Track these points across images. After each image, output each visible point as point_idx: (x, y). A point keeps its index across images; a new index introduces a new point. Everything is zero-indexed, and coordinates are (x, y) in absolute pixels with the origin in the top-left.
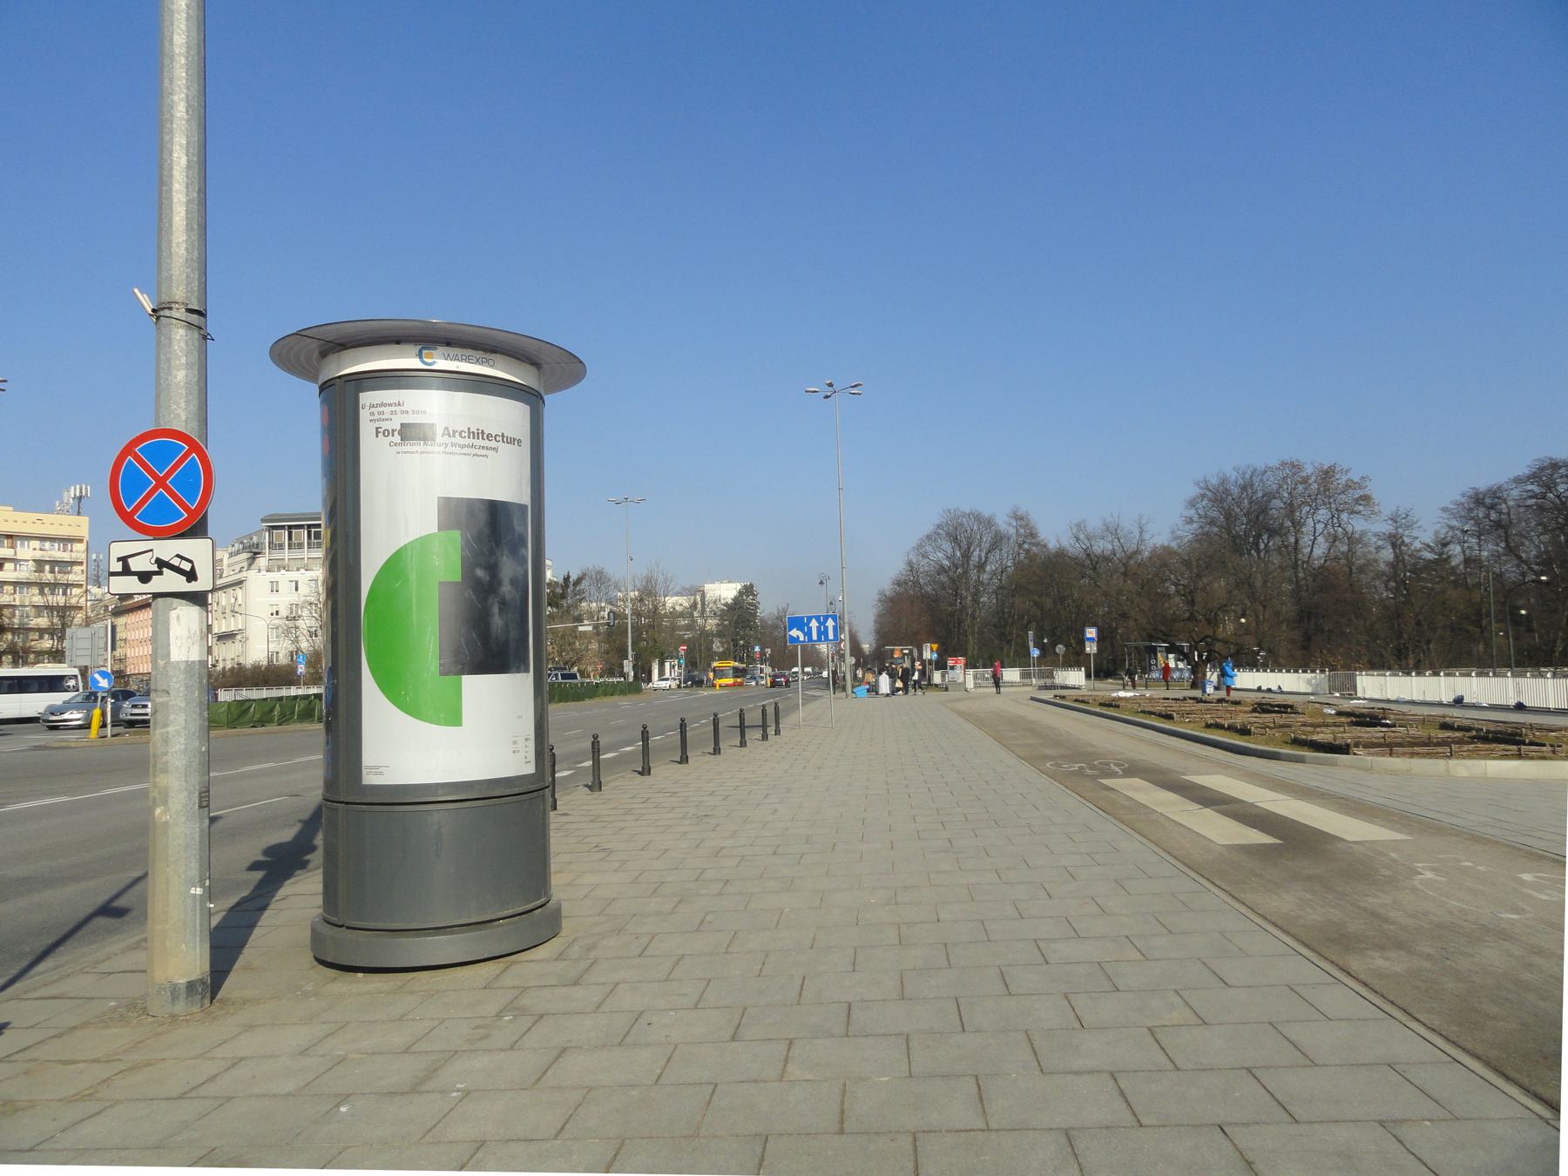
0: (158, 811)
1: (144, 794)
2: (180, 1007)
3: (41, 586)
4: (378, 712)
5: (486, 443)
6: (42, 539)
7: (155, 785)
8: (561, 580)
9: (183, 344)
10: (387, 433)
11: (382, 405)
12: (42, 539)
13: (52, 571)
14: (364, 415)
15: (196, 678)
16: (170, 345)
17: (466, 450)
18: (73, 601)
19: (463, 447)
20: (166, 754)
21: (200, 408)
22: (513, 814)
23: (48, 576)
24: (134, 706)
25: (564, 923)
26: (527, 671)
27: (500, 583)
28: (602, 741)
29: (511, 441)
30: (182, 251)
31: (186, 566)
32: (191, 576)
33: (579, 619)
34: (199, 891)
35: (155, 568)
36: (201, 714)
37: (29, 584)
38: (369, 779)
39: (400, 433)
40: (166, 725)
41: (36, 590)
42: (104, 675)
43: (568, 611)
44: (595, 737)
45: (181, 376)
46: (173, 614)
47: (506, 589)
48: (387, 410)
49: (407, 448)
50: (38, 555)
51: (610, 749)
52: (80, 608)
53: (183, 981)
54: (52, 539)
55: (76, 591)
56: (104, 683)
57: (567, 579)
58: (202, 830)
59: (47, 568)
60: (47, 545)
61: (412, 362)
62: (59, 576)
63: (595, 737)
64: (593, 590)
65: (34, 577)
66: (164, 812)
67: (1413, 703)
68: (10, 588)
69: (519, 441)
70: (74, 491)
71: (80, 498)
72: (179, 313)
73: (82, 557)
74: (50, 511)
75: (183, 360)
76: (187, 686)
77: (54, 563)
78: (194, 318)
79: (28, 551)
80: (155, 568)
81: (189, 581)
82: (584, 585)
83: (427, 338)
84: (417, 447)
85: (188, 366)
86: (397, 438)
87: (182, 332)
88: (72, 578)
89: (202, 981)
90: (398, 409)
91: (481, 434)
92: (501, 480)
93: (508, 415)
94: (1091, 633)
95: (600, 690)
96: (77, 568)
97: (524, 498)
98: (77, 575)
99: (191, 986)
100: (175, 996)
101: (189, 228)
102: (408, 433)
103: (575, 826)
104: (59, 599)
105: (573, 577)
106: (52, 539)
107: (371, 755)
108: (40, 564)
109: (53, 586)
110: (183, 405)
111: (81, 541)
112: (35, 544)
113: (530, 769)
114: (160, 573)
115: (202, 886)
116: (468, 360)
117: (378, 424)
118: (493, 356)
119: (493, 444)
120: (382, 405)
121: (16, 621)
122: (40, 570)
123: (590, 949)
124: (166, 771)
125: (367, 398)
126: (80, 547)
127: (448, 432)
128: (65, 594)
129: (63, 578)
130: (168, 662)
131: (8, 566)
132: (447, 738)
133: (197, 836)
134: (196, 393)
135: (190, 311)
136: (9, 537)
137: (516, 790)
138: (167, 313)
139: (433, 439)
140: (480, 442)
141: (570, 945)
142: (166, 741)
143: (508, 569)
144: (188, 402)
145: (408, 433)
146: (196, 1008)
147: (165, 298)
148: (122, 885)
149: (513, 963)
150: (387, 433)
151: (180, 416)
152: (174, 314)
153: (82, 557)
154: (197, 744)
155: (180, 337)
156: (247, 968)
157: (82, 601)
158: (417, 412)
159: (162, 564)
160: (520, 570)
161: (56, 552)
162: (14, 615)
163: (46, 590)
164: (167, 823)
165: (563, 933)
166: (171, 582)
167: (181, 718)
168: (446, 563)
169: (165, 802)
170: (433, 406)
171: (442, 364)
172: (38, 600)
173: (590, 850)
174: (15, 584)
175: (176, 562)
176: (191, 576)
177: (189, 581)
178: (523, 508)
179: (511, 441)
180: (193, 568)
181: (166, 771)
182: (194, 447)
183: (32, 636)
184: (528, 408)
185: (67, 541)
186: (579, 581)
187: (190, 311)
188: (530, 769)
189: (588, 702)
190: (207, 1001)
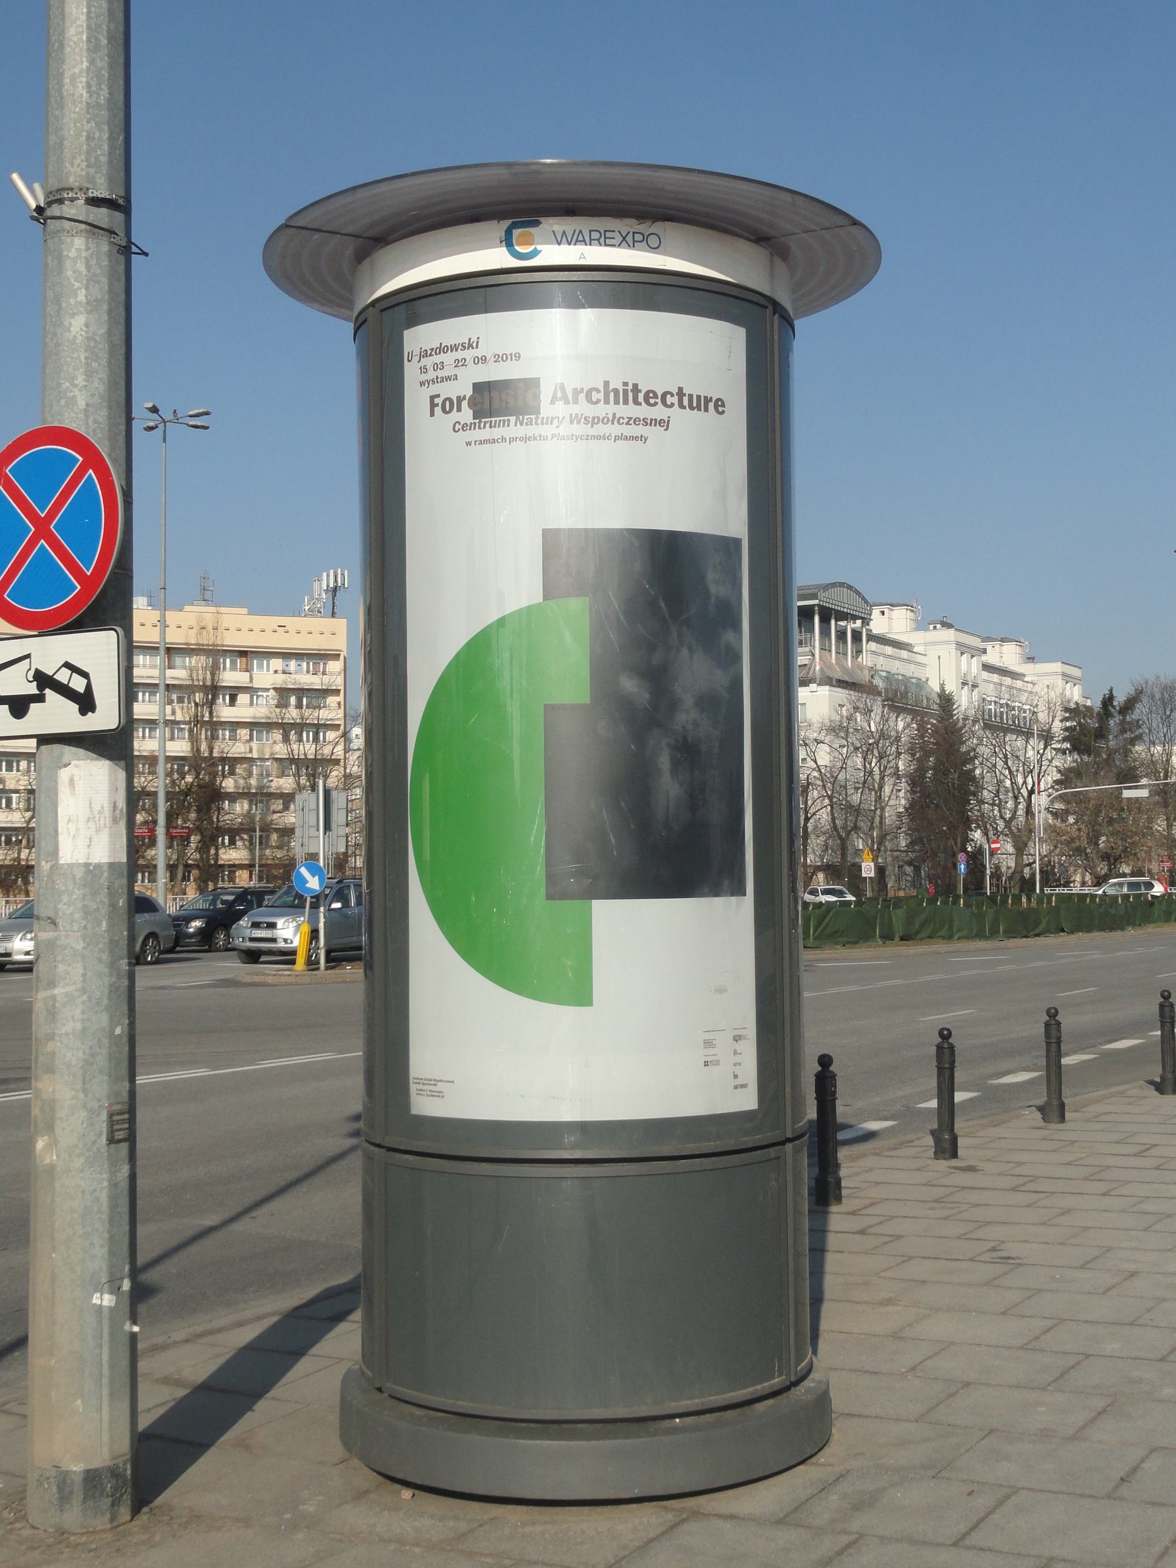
0: (40, 1144)
1: (26, 1106)
2: (72, 1517)
3: (286, 728)
4: (435, 964)
5: (643, 411)
6: (286, 655)
7: (38, 1093)
8: (1095, 703)
9: (81, 267)
10: (450, 406)
11: (442, 349)
12: (286, 655)
13: (299, 706)
14: (411, 372)
15: (103, 897)
16: (60, 270)
17: (601, 429)
18: (327, 751)
19: (595, 421)
20: (51, 1037)
21: (112, 385)
22: (758, 1188)
23: (292, 714)
24: (256, 925)
25: (840, 1432)
26: (740, 891)
27: (674, 706)
28: (1067, 1020)
29: (700, 403)
30: (81, 90)
31: (78, 684)
32: (86, 702)
33: (1129, 776)
34: (108, 1300)
35: (32, 689)
36: (112, 965)
37: (268, 726)
38: (425, 1105)
39: (472, 403)
40: (52, 984)
41: (277, 735)
42: (314, 870)
43: (1109, 761)
44: (1052, 1014)
45: (80, 324)
46: (64, 774)
47: (687, 717)
48: (449, 358)
49: (486, 433)
50: (280, 680)
51: (1085, 1040)
52: (337, 762)
53: (78, 1468)
54: (299, 656)
55: (331, 735)
56: (314, 883)
57: (1108, 701)
58: (114, 1185)
59: (293, 700)
60: (293, 664)
61: (495, 257)
62: (307, 712)
63: (1052, 1014)
64: (1156, 721)
65: (275, 715)
66: (49, 1147)
67: (606, 164)
68: (243, 733)
69: (719, 404)
70: (326, 580)
71: (335, 589)
72: (77, 209)
73: (338, 682)
74: (297, 613)
75: (82, 296)
76: (86, 912)
77: (300, 692)
78: (102, 215)
79: (267, 675)
80: (32, 689)
81: (83, 712)
82: (1140, 711)
83: (521, 206)
84: (512, 428)
85: (92, 306)
86: (466, 415)
87: (79, 242)
88: (324, 714)
89: (114, 1473)
90: (468, 354)
91: (632, 393)
92: (691, 486)
93: (706, 351)
94: (96, 1300)
95: (1156, 910)
96: (332, 700)
97: (730, 518)
98: (331, 710)
99: (92, 1478)
100: (64, 1498)
101: (93, 47)
102: (491, 401)
103: (975, 1197)
104: (306, 748)
105: (1120, 698)
106: (299, 656)
107: (426, 1057)
108: (283, 693)
109: (300, 727)
110: (80, 380)
111: (336, 657)
112: (277, 663)
113: (748, 1101)
114: (40, 698)
115: (116, 1290)
116: (604, 240)
117: (434, 389)
118: (657, 228)
119: (659, 412)
120: (442, 349)
121: (253, 782)
122: (282, 704)
123: (858, 1506)
124: (51, 1070)
125: (419, 337)
126: (335, 666)
127: (561, 394)
128: (316, 739)
129: (312, 716)
130: (55, 867)
131: (243, 698)
132: (602, 1028)
133: (104, 1196)
134: (104, 356)
135: (95, 202)
136: (243, 654)
137: (731, 1144)
138: (55, 210)
139: (537, 411)
140: (631, 410)
141: (825, 1488)
142: (52, 1014)
143: (694, 674)
144: (89, 375)
145: (491, 401)
146: (102, 1522)
147: (54, 184)
148: (173, 1242)
149: (696, 1514)
150: (450, 406)
151: (79, 403)
152: (68, 210)
153: (338, 682)
154: (104, 1019)
155: (79, 257)
156: (243, 1444)
157: (339, 751)
158: (498, 358)
159: (43, 680)
160: (721, 679)
161: (304, 677)
162: (250, 774)
163: (293, 736)
164: (52, 1167)
165: (821, 1458)
166: (54, 713)
167: (76, 971)
168: (565, 667)
169: (50, 1128)
170: (558, 347)
171: (552, 254)
172: (281, 750)
173: (905, 1283)
174: (252, 725)
175: (63, 676)
176: (86, 702)
177: (83, 712)
178: (729, 545)
179: (700, 403)
180: (89, 687)
181: (51, 1070)
182: (92, 457)
183: (278, 805)
184: (740, 333)
185: (319, 657)
186: (1129, 705)
187: (95, 202)
188: (748, 1101)
189: (1131, 932)
190: (124, 1512)
